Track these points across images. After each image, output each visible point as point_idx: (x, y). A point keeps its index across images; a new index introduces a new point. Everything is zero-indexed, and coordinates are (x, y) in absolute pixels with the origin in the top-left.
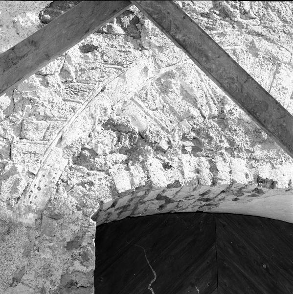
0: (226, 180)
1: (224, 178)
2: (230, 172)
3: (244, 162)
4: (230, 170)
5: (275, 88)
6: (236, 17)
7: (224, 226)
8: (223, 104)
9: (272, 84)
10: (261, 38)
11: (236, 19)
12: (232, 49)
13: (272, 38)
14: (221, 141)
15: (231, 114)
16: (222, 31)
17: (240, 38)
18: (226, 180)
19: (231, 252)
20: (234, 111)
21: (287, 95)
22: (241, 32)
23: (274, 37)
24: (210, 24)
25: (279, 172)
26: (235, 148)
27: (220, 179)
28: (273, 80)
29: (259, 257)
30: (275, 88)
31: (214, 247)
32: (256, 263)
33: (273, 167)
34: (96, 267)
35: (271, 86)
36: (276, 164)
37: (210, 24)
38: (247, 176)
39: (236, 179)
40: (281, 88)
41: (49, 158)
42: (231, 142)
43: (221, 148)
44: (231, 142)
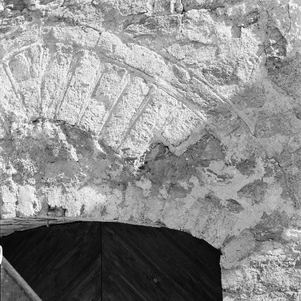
0: (10, 213)
1: (8, 210)
2: (17, 203)
3: (32, 189)
4: (16, 200)
5: (73, 88)
6: (34, 5)
7: (111, 235)
8: (11, 123)
9: (69, 83)
10: (63, 23)
11: (33, 8)
12: (26, 50)
13: (76, 18)
14: (8, 168)
15: (19, 132)
16: (17, 28)
17: (37, 32)
18: (10, 213)
19: (117, 263)
20: (22, 129)
21: (87, 94)
22: (39, 23)
23: (79, 16)
24: (4, 25)
25: (70, 196)
26: (24, 174)
27: (4, 213)
28: (72, 77)
29: (149, 270)
30: (73, 88)
31: (99, 260)
32: (145, 276)
33: (64, 192)
34: (174, 231)
35: (68, 85)
36: (68, 187)
37: (4, 25)
38: (35, 205)
39: (22, 211)
40: (80, 85)
41: (100, 77)
42: (20, 167)
43: (8, 176)
44: (20, 167)
